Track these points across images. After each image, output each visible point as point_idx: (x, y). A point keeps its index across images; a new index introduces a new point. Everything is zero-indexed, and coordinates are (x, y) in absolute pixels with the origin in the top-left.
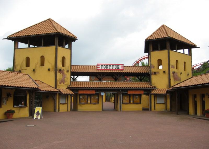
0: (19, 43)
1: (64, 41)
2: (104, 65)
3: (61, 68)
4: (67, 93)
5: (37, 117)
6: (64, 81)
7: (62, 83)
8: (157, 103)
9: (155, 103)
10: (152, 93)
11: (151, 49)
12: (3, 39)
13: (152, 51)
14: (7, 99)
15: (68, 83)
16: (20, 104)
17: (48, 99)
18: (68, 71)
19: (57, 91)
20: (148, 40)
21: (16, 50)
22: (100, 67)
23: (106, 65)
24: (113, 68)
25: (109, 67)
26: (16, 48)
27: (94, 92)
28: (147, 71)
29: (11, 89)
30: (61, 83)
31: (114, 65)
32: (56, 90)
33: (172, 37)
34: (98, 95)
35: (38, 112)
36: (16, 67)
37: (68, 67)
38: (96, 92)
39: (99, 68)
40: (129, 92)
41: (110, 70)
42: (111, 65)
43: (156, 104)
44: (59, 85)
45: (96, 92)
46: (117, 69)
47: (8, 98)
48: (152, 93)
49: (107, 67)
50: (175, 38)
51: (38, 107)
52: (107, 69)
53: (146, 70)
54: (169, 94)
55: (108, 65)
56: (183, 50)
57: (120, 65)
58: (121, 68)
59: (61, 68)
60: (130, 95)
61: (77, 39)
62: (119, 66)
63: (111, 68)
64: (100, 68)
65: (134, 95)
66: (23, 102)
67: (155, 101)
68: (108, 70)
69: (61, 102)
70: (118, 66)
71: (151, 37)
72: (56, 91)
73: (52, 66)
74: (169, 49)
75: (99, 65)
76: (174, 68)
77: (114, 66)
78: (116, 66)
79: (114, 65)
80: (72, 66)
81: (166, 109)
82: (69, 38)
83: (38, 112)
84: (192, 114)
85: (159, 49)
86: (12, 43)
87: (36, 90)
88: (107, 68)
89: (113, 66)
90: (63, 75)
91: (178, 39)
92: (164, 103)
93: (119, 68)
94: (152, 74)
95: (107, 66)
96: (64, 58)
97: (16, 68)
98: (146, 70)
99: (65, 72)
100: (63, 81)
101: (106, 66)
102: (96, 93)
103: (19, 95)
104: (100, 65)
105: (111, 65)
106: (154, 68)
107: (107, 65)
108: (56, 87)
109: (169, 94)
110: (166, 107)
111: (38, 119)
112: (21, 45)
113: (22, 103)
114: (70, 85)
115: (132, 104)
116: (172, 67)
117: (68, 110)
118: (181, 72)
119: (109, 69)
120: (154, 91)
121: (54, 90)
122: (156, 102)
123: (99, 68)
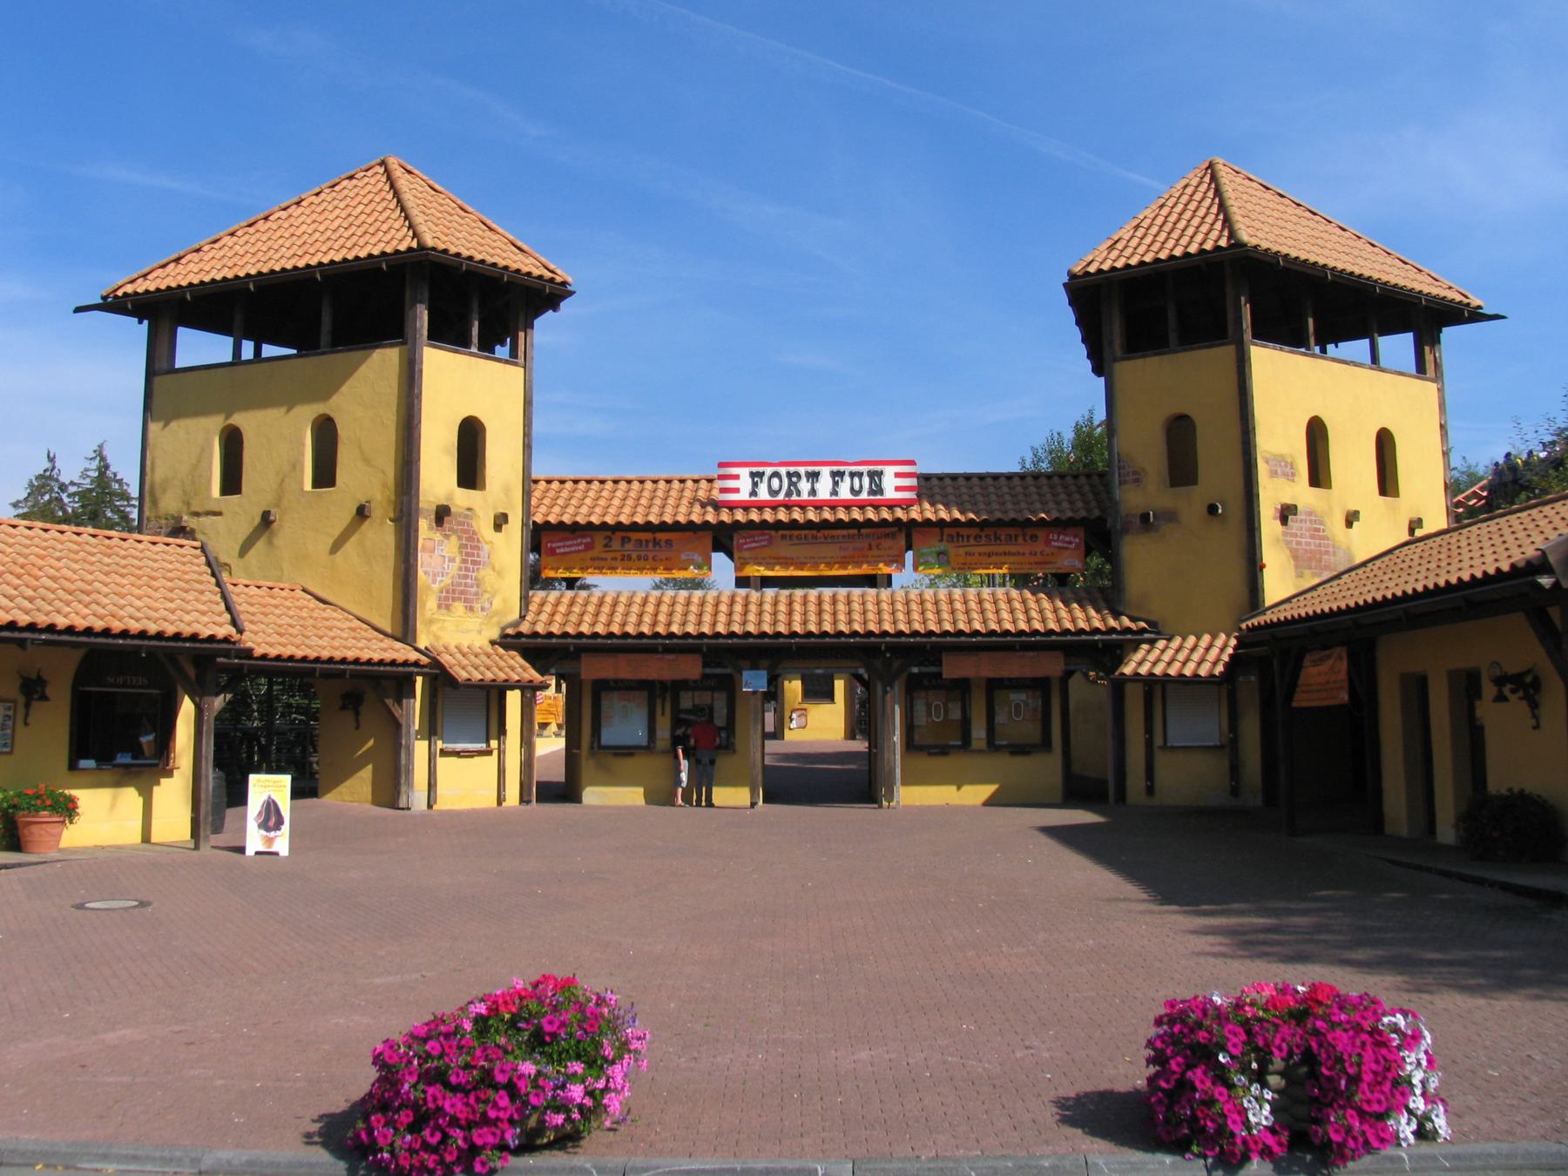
0: (182, 332)
1: (475, 306)
2: (769, 471)
3: (450, 496)
4: (489, 676)
5: (270, 841)
6: (474, 589)
7: (459, 607)
8: (1164, 747)
9: (1149, 744)
10: (1128, 670)
11: (1111, 343)
12: (78, 310)
13: (1119, 353)
14: (21, 710)
15: (505, 601)
16: (123, 750)
17: (357, 714)
18: (500, 521)
19: (416, 664)
20: (1087, 273)
21: (157, 380)
22: (744, 484)
23: (783, 470)
24: (834, 492)
25: (805, 486)
26: (162, 364)
27: (691, 668)
28: (1093, 504)
29: (21, 643)
30: (448, 607)
31: (848, 469)
32: (402, 652)
33: (1264, 245)
34: (728, 685)
35: (271, 808)
36: (158, 493)
37: (507, 490)
38: (708, 671)
39: (737, 490)
40: (953, 668)
41: (818, 506)
42: (825, 472)
43: (1161, 759)
44: (431, 622)
45: (708, 671)
46: (864, 496)
47: (27, 706)
48: (1128, 670)
49: (791, 483)
50: (1293, 254)
51: (270, 771)
52: (794, 497)
53: (1086, 503)
54: (1253, 678)
55: (802, 470)
56: (1364, 344)
57: (889, 471)
58: (898, 489)
59: (450, 496)
60: (962, 687)
61: (572, 293)
62: (880, 474)
63: (824, 489)
64: (744, 495)
65: (994, 686)
66: (144, 740)
67: (1149, 730)
68: (803, 506)
69: (609, 736)
70: (871, 475)
71: (1114, 254)
72: (406, 663)
73: (385, 486)
74: (1248, 335)
75: (734, 471)
76: (1291, 476)
77: (841, 474)
78: (860, 475)
79: (842, 468)
80: (536, 482)
81: (1235, 791)
82: (1286, 270)
83: (271, 808)
84: (1404, 831)
85: (1173, 337)
86: (135, 332)
87: (227, 654)
88: (789, 493)
89: (834, 474)
90: (462, 547)
91: (1312, 259)
92: (1221, 747)
93: (880, 491)
94: (1125, 530)
95: (789, 475)
96: (471, 437)
97: (155, 503)
98: (1090, 496)
99: (484, 527)
100: (460, 594)
101: (785, 481)
102: (705, 676)
103: (112, 686)
104: (744, 472)
105: (825, 472)
106: (1137, 481)
107: (792, 469)
108: (405, 630)
109: (1253, 678)
110: (1235, 770)
111: (276, 854)
112: (198, 348)
113: (140, 745)
114: (522, 617)
115: (980, 751)
116: (1273, 474)
117: (500, 800)
118: (1353, 508)
119: (805, 496)
120: (1138, 656)
121: (388, 656)
122: (1158, 741)
123: (737, 490)
